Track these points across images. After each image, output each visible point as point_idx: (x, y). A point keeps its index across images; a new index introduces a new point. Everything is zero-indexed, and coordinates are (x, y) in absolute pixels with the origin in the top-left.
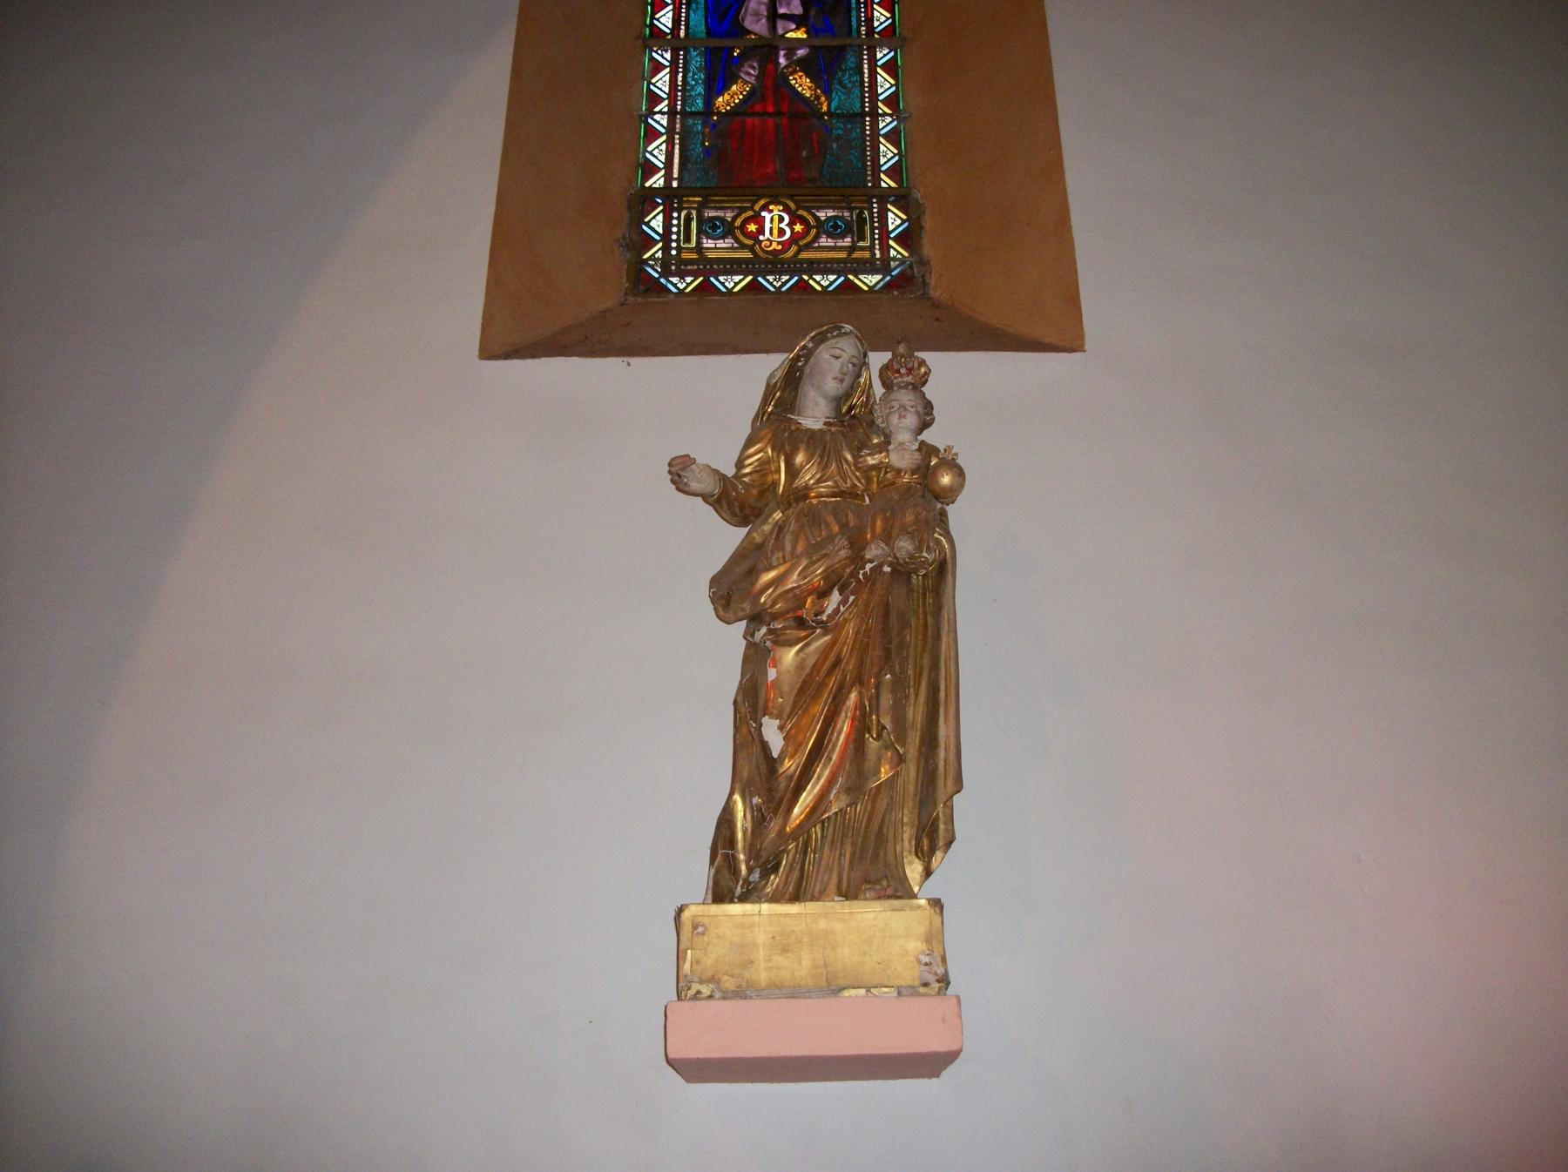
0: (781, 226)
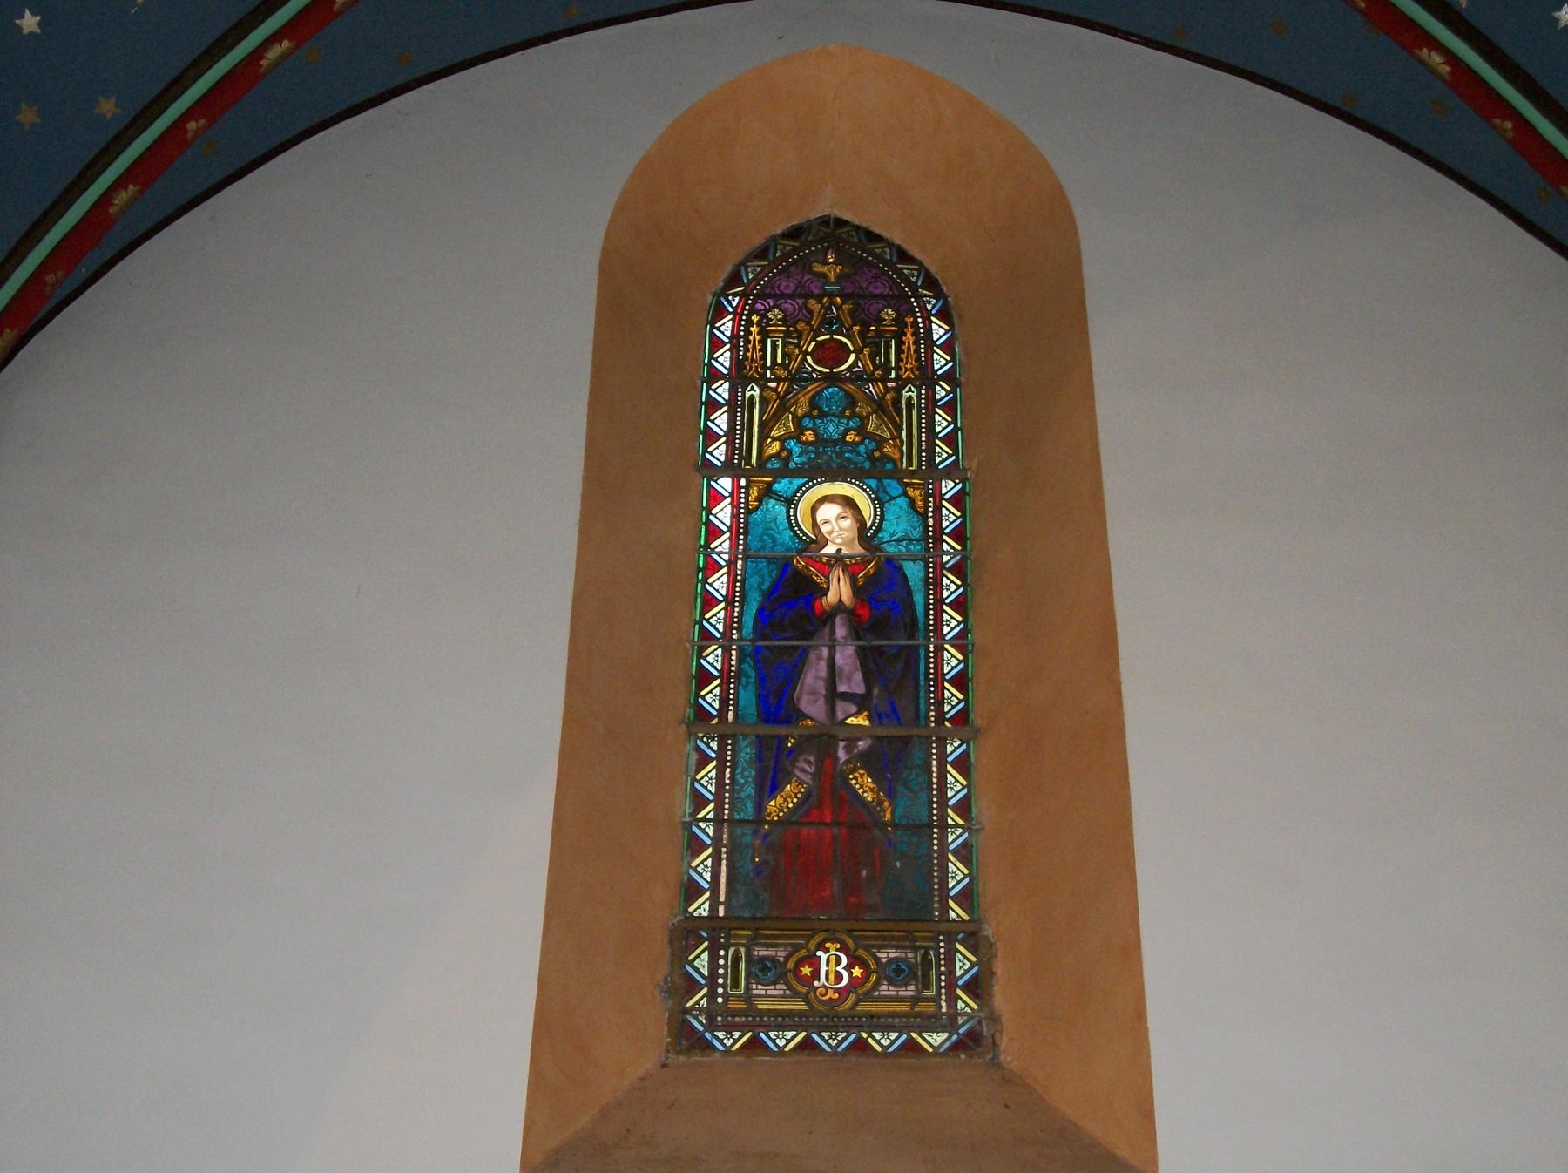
0: (837, 969)
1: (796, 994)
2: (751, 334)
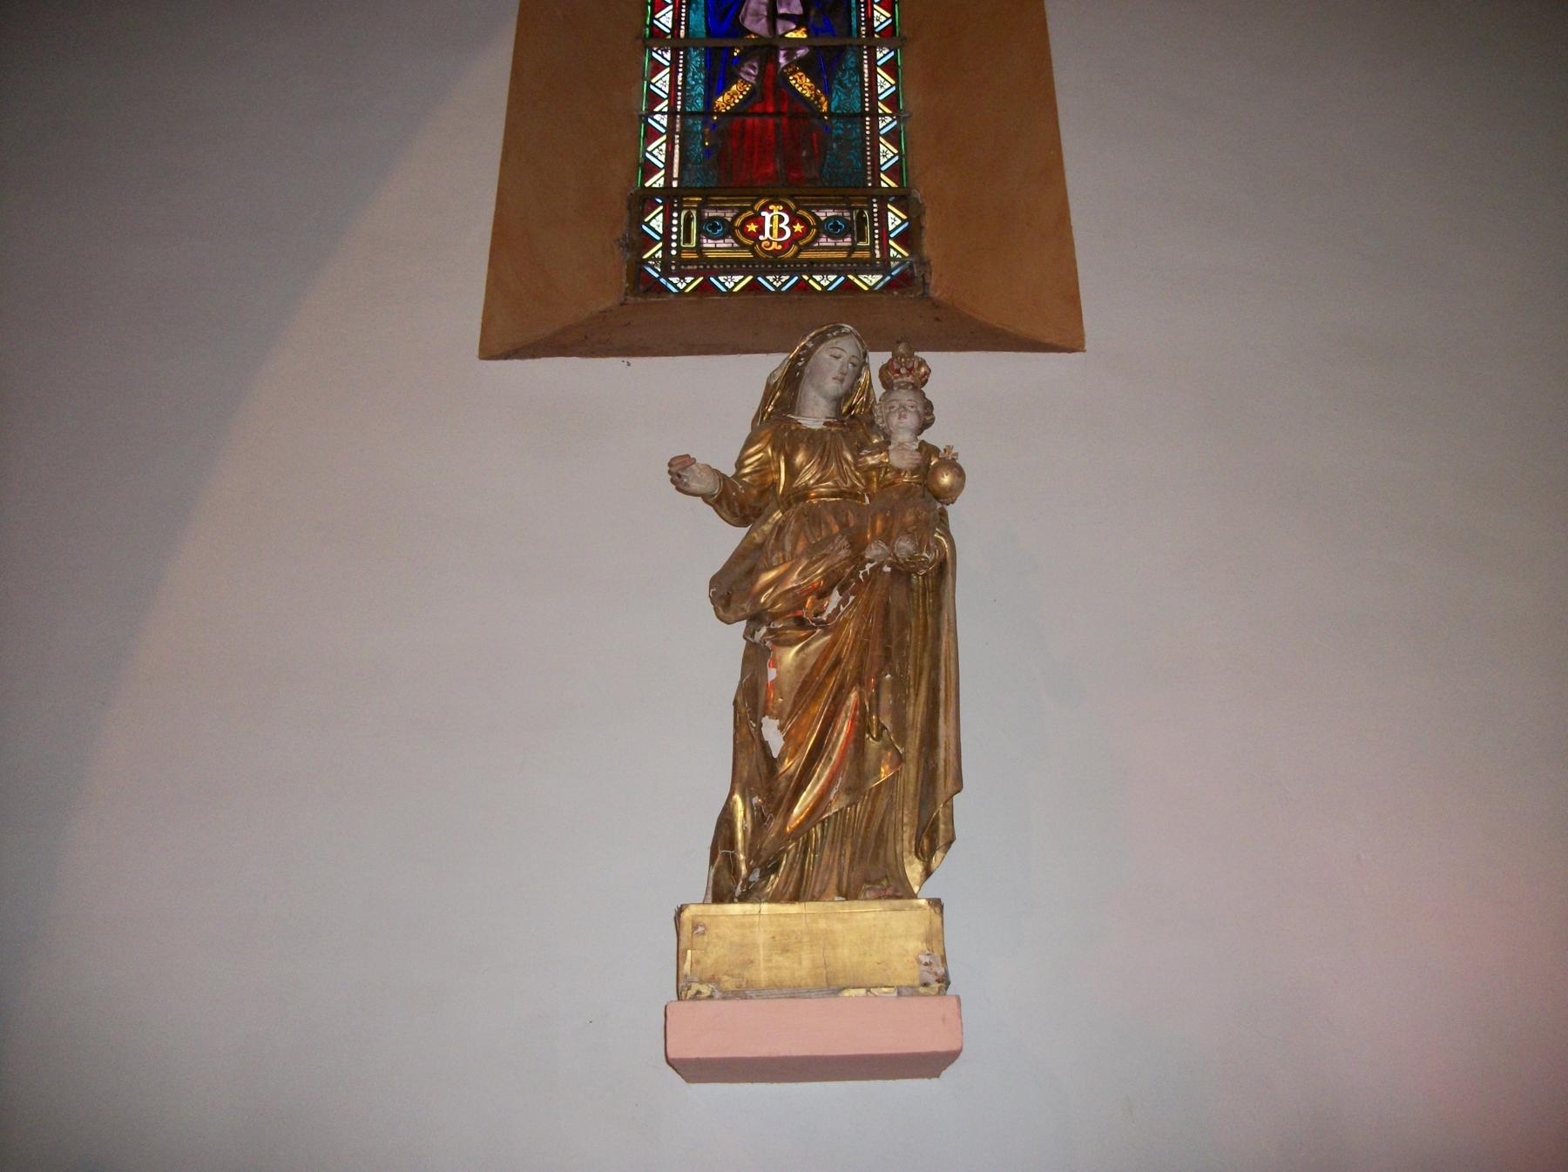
0: (781, 226)
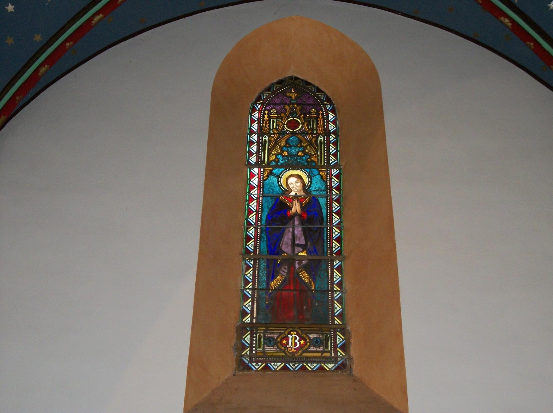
0: (295, 341)
1: (281, 350)
2: (265, 118)
